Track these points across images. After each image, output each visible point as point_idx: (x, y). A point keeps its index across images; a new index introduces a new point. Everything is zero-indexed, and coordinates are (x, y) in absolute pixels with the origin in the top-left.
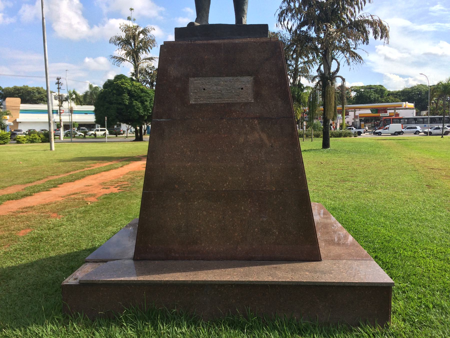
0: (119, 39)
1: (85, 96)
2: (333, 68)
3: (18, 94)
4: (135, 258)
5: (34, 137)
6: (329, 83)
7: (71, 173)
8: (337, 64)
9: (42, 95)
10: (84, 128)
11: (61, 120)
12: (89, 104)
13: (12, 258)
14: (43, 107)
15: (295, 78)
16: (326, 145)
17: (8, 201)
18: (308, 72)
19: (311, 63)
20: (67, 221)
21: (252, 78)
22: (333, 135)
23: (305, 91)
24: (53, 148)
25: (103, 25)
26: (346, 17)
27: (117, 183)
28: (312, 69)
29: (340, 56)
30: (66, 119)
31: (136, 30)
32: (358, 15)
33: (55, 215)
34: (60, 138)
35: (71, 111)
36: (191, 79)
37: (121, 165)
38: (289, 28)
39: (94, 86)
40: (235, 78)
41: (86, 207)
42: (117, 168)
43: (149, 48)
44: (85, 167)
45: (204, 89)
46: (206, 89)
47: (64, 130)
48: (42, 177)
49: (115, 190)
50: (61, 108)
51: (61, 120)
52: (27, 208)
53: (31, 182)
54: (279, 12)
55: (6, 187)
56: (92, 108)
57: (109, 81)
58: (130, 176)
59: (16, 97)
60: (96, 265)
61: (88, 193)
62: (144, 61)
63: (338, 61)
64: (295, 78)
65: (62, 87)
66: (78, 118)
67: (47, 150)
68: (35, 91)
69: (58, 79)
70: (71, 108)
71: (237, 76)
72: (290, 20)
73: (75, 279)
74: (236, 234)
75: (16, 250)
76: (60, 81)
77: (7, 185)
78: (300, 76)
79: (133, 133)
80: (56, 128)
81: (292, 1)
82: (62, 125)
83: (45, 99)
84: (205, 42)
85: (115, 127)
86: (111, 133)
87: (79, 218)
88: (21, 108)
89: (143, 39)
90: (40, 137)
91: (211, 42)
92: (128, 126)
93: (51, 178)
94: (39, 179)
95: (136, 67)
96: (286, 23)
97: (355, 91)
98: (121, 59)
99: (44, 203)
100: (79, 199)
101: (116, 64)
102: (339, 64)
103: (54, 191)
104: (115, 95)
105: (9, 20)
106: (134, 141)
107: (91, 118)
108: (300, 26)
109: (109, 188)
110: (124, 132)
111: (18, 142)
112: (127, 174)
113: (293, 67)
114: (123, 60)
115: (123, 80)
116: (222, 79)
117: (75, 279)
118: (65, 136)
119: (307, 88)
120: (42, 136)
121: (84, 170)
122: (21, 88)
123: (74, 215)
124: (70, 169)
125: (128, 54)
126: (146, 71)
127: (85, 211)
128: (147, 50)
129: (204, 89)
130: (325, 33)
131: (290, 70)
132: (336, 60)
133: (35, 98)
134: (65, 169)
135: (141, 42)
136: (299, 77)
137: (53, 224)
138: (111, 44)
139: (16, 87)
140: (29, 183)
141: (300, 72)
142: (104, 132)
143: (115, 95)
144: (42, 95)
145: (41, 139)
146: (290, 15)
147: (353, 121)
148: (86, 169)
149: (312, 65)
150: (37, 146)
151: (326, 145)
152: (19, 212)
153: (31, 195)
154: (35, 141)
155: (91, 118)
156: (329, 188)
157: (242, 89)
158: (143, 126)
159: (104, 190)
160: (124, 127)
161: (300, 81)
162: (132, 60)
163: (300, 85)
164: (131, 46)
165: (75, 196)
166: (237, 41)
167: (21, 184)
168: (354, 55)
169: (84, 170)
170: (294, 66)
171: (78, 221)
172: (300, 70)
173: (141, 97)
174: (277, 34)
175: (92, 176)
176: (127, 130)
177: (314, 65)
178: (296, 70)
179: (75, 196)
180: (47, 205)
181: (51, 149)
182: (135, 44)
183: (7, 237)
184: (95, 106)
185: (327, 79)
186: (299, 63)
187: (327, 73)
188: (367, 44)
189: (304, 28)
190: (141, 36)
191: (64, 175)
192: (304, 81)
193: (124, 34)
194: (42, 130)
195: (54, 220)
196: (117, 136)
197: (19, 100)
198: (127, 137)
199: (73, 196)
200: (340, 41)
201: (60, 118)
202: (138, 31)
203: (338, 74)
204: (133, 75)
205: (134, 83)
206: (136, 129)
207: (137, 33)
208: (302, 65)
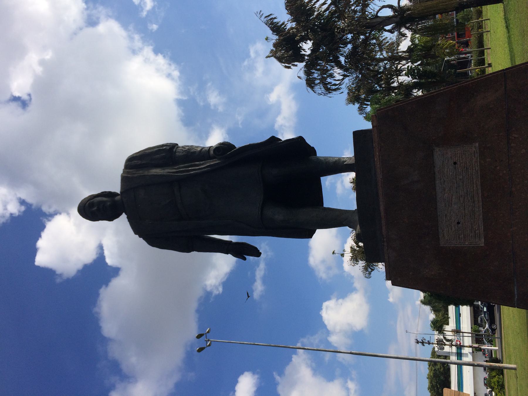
0: (366, 268)
1: (435, 310)
2: (388, 13)
5: (496, 383)
6: (409, 14)
8: (384, 9)
10: (479, 319)
11: (470, 347)
12: (447, 311)
14: (454, 369)
18: (393, 43)
19: (382, 41)
21: (437, 149)
23: (417, 41)
25: (352, 277)
26: (328, 12)
28: (388, 39)
31: (355, 250)
34: (496, 351)
35: (457, 331)
36: (442, 243)
38: (341, 77)
45: (458, 223)
46: (459, 219)
47: (484, 344)
51: (470, 347)
56: (452, 309)
63: (378, 8)
64: (401, 59)
65: (427, 339)
66: (466, 325)
69: (418, 342)
70: (453, 331)
71: (434, 173)
78: (397, 53)
80: (481, 353)
82: (476, 345)
84: (383, 222)
90: (495, 376)
91: (382, 214)
96: (338, 82)
102: (384, 7)
105: (354, 374)
108: (340, 66)
113: (387, 63)
119: (412, 40)
122: (431, 382)
129: (458, 223)
131: (391, 67)
133: (442, 369)
139: (429, 389)
145: (498, 374)
146: (329, 80)
149: (384, 40)
150: (508, 382)
154: (501, 383)
157: (455, 163)
161: (404, 52)
163: (410, 50)
166: (380, 177)
170: (386, 62)
172: (390, 54)
174: (349, 90)
177: (383, 38)
178: (390, 59)
181: (515, 369)
184: (450, 304)
186: (381, 57)
187: (394, 19)
189: (342, 59)
192: (405, 45)
193: (360, 262)
197: (445, 390)
200: (355, 12)
201: (467, 347)
202: (355, 248)
203: (395, 4)
207: (358, 249)
208: (384, 53)
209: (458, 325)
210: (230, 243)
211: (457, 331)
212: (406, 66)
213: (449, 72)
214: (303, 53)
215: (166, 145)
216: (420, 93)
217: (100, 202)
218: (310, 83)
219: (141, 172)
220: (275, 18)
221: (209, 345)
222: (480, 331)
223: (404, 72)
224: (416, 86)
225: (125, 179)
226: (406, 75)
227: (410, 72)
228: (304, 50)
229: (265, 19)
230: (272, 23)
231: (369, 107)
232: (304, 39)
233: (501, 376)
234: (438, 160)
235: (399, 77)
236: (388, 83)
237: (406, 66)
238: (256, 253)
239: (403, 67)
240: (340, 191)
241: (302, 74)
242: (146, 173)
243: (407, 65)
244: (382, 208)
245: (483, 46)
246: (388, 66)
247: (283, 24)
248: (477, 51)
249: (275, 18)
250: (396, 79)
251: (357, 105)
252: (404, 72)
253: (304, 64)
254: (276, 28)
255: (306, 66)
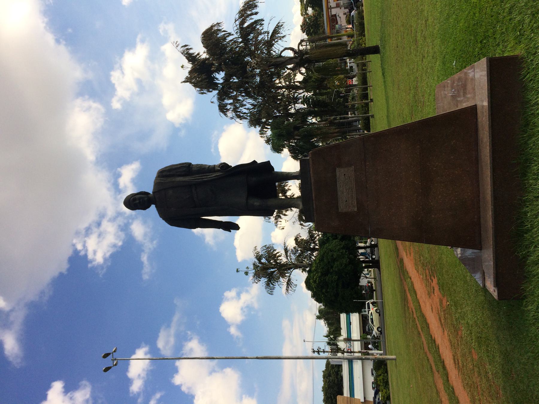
0: (268, 285)
3: (332, 400)
4: (481, 249)
5: (382, 381)
7: (420, 330)
9: (331, 372)
10: (367, 327)
13: (494, 357)
15: (297, 88)
16: (375, 50)
17: (450, 382)
20: (464, 320)
22: (362, 33)
24: (394, 357)
27: (428, 281)
29: (277, 48)
30: (357, 346)
32: (235, 35)
33: (460, 333)
36: (340, 210)
37: (409, 279)
39: (318, 314)
40: (338, 180)
41: (451, 306)
42: (412, 283)
43: (275, 252)
44: (413, 317)
48: (426, 358)
49: (435, 281)
50: (345, 350)
52: (455, 361)
53: (431, 368)
54: (238, 120)
55: (437, 390)
56: (343, 316)
57: (313, 296)
58: (420, 267)
59: (336, 401)
60: (486, 278)
61: (439, 307)
62: (289, 258)
64: (297, 88)
67: (396, 364)
68: (328, 380)
72: (245, 107)
73: (495, 291)
74: (457, 172)
75: (488, 356)
76: (316, 350)
77: (435, 390)
78: (294, 82)
79: (370, 271)
81: (226, 106)
83: (336, 369)
85: (364, 292)
86: (372, 298)
87: (461, 309)
88: (349, 396)
89: (266, 260)
90: (381, 375)
92: (362, 278)
93: (426, 349)
94: (428, 360)
95: (296, 267)
97: (306, 10)
98: (289, 283)
99: (450, 346)
100: (445, 315)
101: (294, 289)
103: (439, 341)
104: (328, 290)
106: (380, 270)
107: (355, 318)
109: (433, 287)
110: (369, 282)
111: (388, 398)
112: (418, 271)
114: (289, 280)
115: (311, 281)
116: (338, 189)
117: (495, 291)
118: (378, 350)
120: (380, 372)
121: (416, 318)
123: (459, 315)
124: (416, 333)
125: (283, 276)
126: (299, 256)
127: (455, 305)
128: (278, 255)
130: (256, 69)
132: (282, 52)
133: (336, 381)
134: (416, 338)
135: (269, 262)
136: (296, 84)
137: (467, 331)
138: (274, 293)
140: (432, 369)
141: (290, 82)
142: (371, 305)
143: (328, 290)
144: (331, 372)
147: (343, 8)
148: (415, 316)
150: (391, 377)
151: (375, 50)
152: (459, 367)
153: (443, 362)
155: (355, 318)
156: (424, 60)
158: (361, 260)
159: (435, 292)
160: (363, 282)
161: (299, 82)
162: (289, 271)
164: (274, 272)
165: (442, 318)
167: (433, 376)
168: (276, 31)
169: (416, 318)
170: (284, 90)
171: (464, 310)
172: (287, 83)
173: (329, 262)
175: (422, 307)
176: (367, 278)
178: (288, 87)
179: (442, 318)
180: (451, 343)
181: (395, 359)
182: (273, 268)
183: (479, 368)
185: (302, 59)
188: (264, 21)
190: (263, 260)
191: (423, 337)
192: (299, 78)
193: (263, 279)
194: (373, 374)
195: (464, 332)
196: (375, 290)
197: (339, 397)
198: (375, 278)
199: (443, 321)
204: (304, 270)
205: (313, 269)
206: (365, 267)
209: (349, 333)
210: (221, 222)
211: (349, 340)
212: (302, 95)
213: (339, 101)
214: (217, 82)
215: (185, 163)
216: (314, 120)
217: (140, 199)
218: (223, 109)
219: (169, 180)
220: (191, 49)
221: (116, 365)
222: (367, 339)
223: (300, 101)
224: (310, 113)
225: (157, 184)
226: (302, 103)
227: (305, 100)
228: (217, 79)
229: (182, 48)
230: (187, 53)
231: (269, 130)
232: (218, 70)
233: (386, 374)
234: (338, 174)
235: (296, 105)
236: (286, 110)
237: (302, 95)
238: (236, 227)
239: (300, 96)
240: (294, 188)
241: (215, 100)
242: (174, 180)
243: (303, 94)
244: (313, 195)
245: (367, 84)
246: (286, 93)
247: (198, 54)
248: (361, 88)
249: (191, 49)
250: (293, 106)
251: (258, 128)
252: (300, 101)
253: (217, 92)
254: (191, 58)
255: (218, 94)
